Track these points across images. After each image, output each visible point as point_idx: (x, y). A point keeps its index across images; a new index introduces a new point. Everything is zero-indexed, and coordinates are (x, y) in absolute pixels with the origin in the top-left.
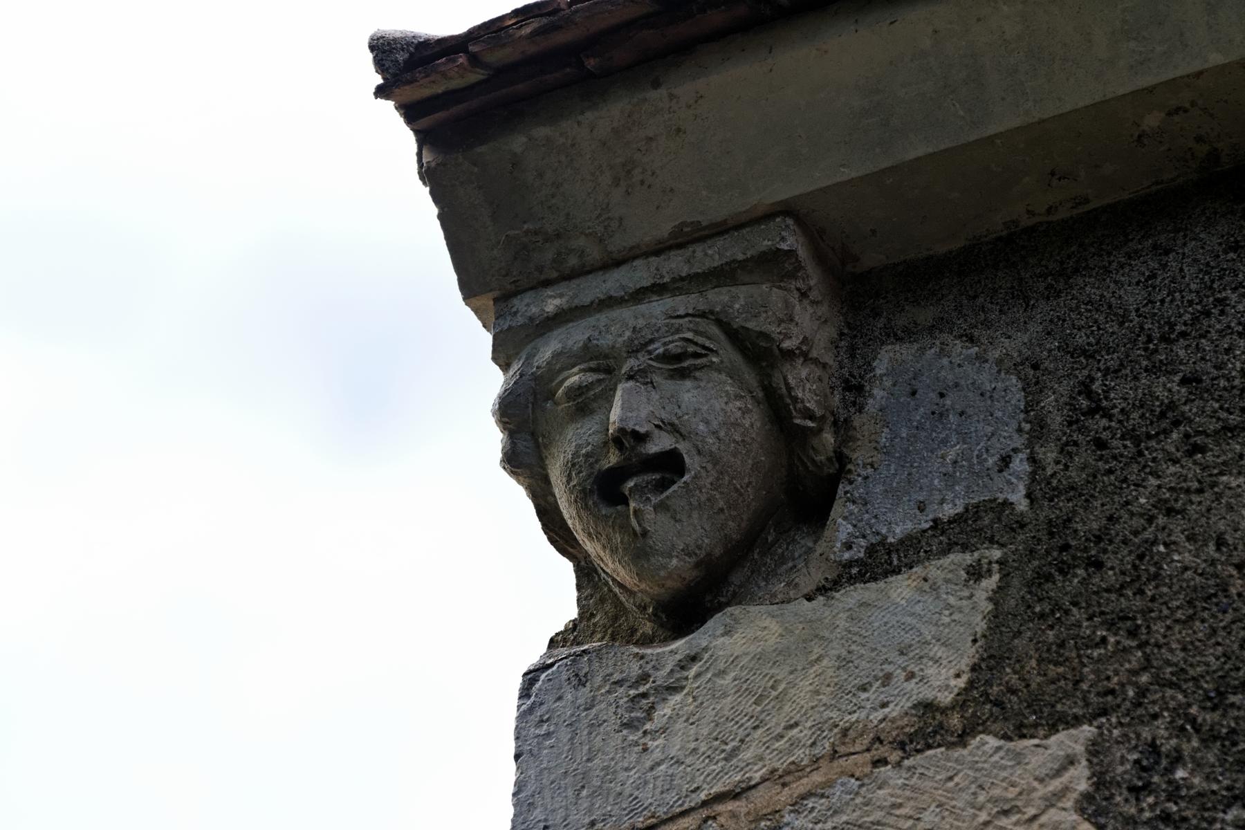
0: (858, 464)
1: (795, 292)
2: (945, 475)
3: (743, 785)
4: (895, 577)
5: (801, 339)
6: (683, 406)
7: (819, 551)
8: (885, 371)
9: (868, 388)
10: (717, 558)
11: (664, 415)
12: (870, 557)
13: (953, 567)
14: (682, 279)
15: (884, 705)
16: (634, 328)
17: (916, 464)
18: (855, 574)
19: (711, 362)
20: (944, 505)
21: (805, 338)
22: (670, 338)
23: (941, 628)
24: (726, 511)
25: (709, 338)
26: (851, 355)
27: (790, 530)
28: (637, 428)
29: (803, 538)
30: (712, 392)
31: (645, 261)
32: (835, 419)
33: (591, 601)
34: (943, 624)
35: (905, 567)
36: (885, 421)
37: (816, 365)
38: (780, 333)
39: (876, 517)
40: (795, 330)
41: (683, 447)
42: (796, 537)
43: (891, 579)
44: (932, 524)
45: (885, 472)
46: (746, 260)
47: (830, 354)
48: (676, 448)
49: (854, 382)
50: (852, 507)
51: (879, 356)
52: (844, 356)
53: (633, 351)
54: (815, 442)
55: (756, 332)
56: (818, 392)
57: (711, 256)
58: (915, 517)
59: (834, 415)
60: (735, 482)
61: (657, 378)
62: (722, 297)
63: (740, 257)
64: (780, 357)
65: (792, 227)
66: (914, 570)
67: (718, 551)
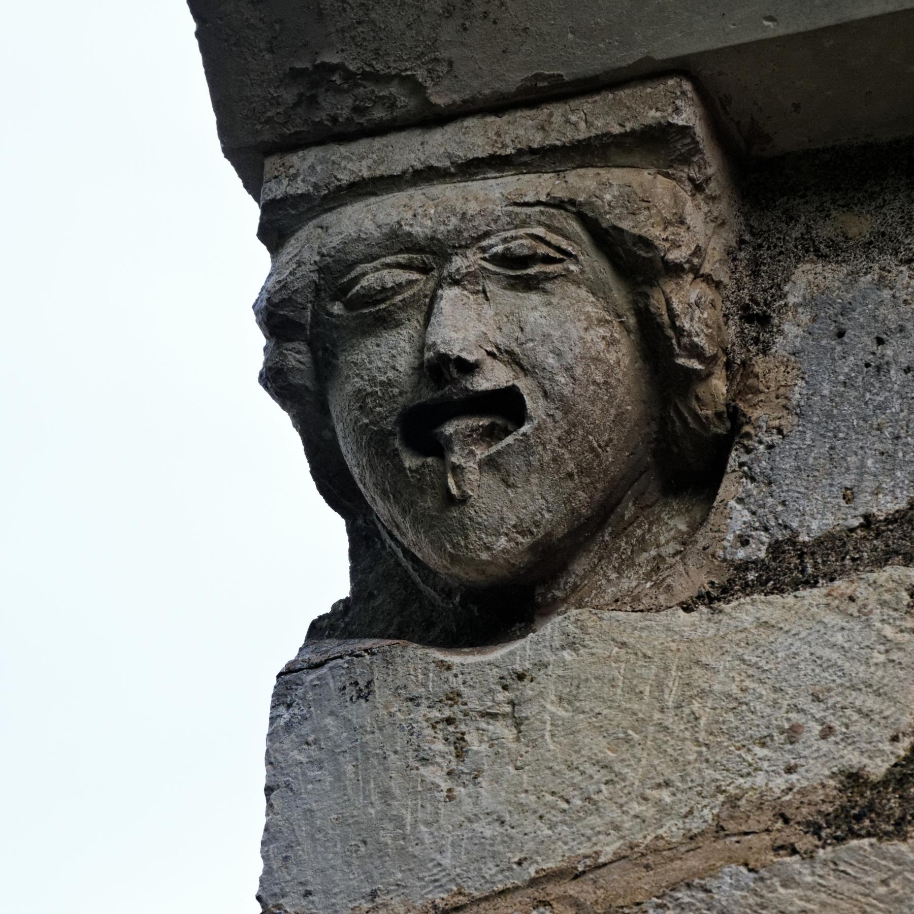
0: (760, 427)
1: (687, 183)
2: (882, 454)
3: (588, 862)
4: (808, 590)
5: (693, 248)
6: (528, 329)
7: (702, 542)
8: (800, 299)
9: (776, 321)
10: (559, 540)
11: (500, 340)
12: (774, 559)
13: (891, 585)
14: (532, 151)
15: (790, 770)
16: (464, 214)
17: (841, 435)
18: (753, 581)
19: (567, 270)
20: (880, 496)
21: (698, 248)
22: (513, 233)
23: (873, 669)
24: (576, 477)
25: (566, 237)
26: (753, 272)
27: (653, 504)
28: (464, 355)
29: (672, 517)
30: (568, 313)
31: (481, 121)
32: (728, 360)
33: (371, 576)
34: (876, 664)
35: (823, 578)
36: (799, 369)
37: (708, 283)
38: (666, 240)
39: (783, 503)
40: (684, 236)
41: (524, 385)
42: (663, 515)
43: (802, 593)
44: (862, 520)
45: (798, 441)
46: (624, 135)
47: (726, 269)
48: (514, 386)
49: (756, 310)
50: (750, 486)
51: (793, 278)
52: (744, 273)
53: (461, 247)
54: (701, 390)
55: (634, 235)
56: (710, 322)
57: (575, 125)
58: (839, 510)
59: (727, 355)
60: (591, 438)
61: (491, 287)
62: (588, 183)
63: (616, 130)
64: (663, 272)
65: (690, 95)
66: (837, 583)
67: (561, 531)
